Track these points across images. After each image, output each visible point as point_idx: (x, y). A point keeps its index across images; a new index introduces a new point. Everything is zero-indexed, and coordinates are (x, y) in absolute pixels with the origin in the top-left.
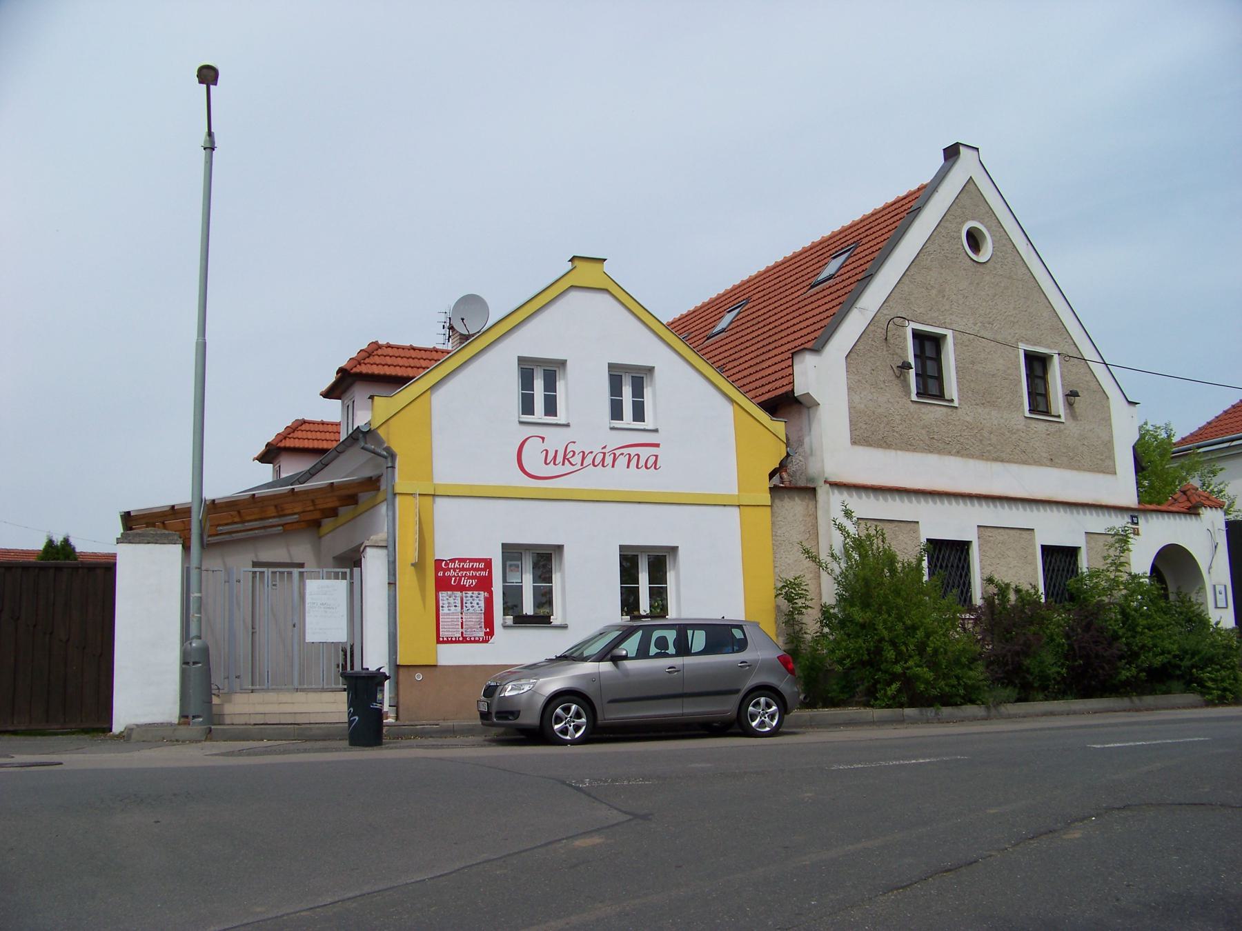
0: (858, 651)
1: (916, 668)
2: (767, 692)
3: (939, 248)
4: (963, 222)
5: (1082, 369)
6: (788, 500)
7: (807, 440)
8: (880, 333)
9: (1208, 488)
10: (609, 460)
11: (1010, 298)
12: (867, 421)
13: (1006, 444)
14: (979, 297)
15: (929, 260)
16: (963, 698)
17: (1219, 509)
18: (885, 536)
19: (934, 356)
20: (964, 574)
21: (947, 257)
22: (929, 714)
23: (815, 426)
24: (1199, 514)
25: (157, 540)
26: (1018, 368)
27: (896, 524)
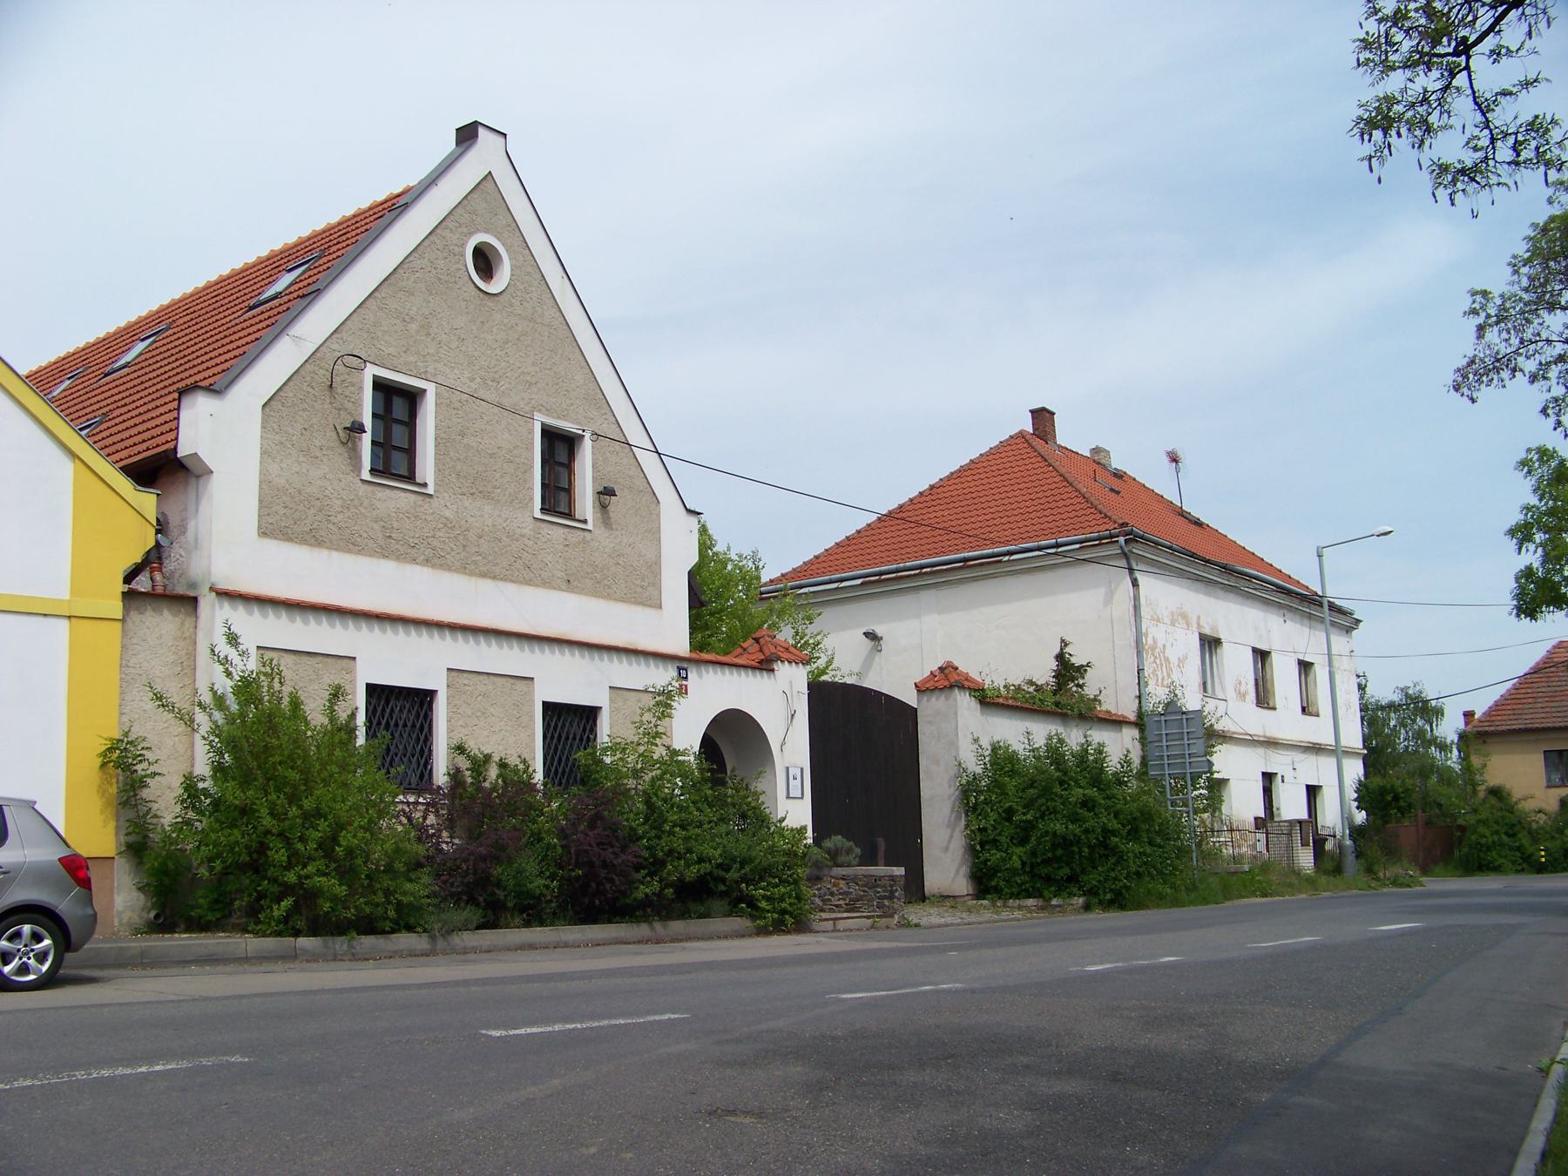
0: (232, 849)
1: (319, 877)
2: (37, 916)
3: (429, 264)
4: (471, 234)
5: (625, 459)
6: (152, 613)
7: (191, 525)
8: (323, 376)
9: (801, 638)
11: (529, 349)
12: (288, 503)
13: (502, 554)
14: (483, 341)
15: (412, 280)
16: (396, 922)
17: (794, 664)
18: (283, 674)
19: (567, 462)
20: (422, 738)
21: (440, 279)
22: (337, 947)
23: (204, 505)
24: (773, 670)
26: (530, 448)
27: (321, 658)
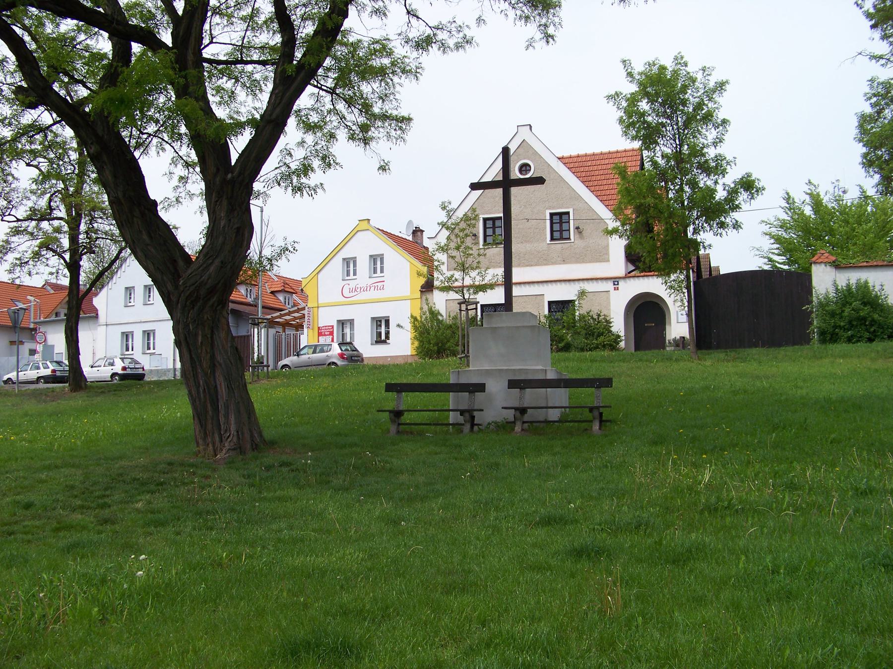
10: (368, 288)
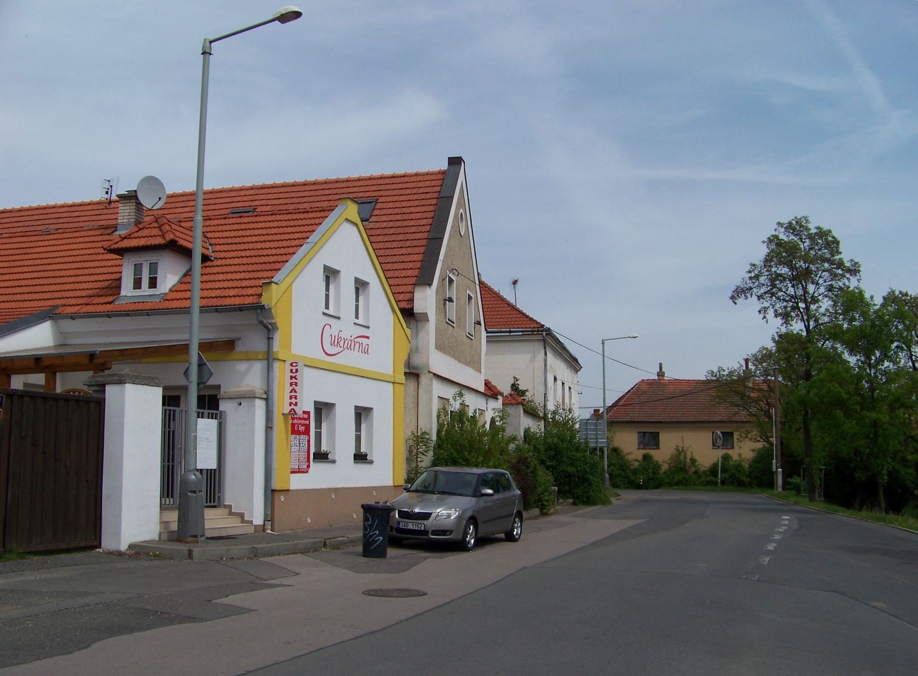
25: (149, 382)
